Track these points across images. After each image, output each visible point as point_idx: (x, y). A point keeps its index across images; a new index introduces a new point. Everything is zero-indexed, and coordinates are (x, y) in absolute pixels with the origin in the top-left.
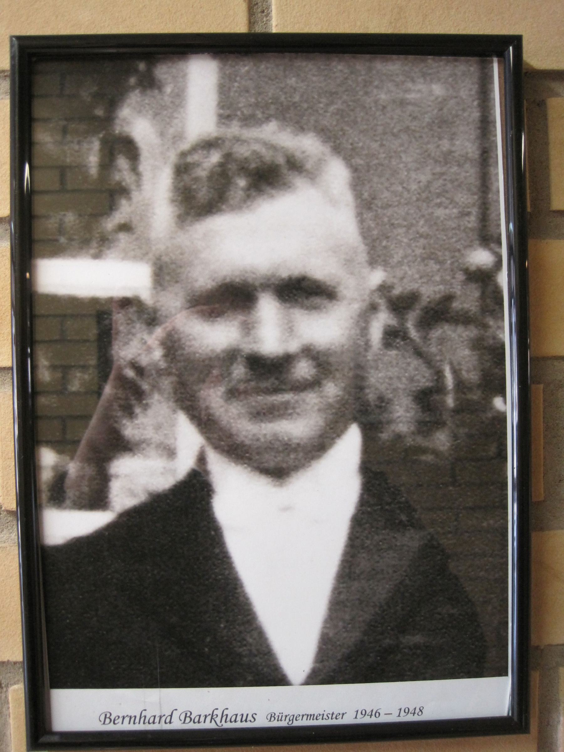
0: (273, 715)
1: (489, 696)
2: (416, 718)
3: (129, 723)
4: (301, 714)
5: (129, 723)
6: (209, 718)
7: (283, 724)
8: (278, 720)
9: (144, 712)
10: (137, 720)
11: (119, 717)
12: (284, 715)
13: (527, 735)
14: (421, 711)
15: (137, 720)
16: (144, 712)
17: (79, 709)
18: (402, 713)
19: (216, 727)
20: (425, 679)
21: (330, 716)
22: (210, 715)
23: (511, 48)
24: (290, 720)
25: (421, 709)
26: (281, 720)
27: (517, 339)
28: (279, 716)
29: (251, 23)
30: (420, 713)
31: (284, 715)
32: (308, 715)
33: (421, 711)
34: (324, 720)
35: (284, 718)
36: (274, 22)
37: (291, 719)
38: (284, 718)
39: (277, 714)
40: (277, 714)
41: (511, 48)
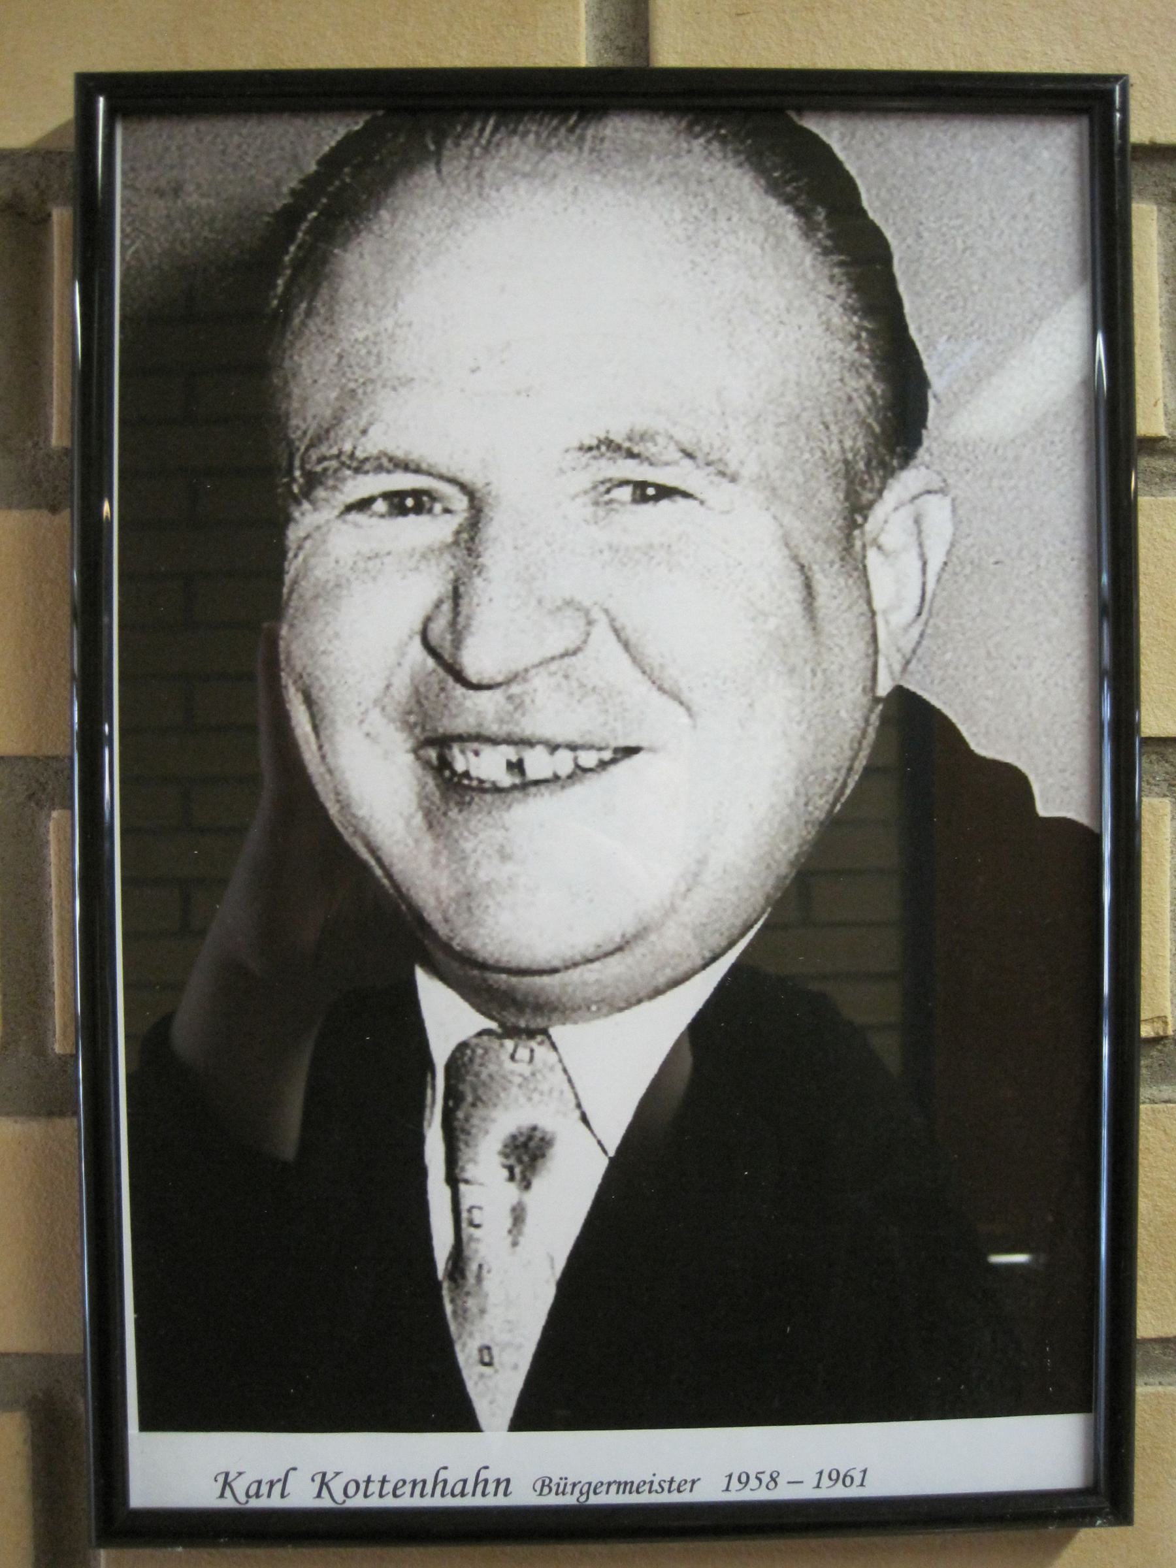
0: (547, 1482)
1: (1038, 1450)
2: (762, 1495)
3: (618, 1492)
4: (689, 1480)
5: (618, 1492)
6: (278, 1488)
7: (569, 1500)
8: (557, 1494)
9: (442, 1472)
10: (429, 1489)
11: (404, 1482)
12: (570, 1481)
13: (1130, 1528)
14: (773, 1479)
15: (429, 1489)
16: (442, 1472)
17: (176, 1469)
18: (825, 1481)
19: (236, 1505)
20: (955, 1417)
21: (666, 1486)
22: (279, 1480)
23: (101, 100)
24: (581, 1494)
25: (775, 1475)
26: (563, 1493)
27: (1112, 749)
28: (559, 1485)
29: (1147, 741)
30: (772, 1485)
31: (570, 1481)
32: (620, 1484)
33: (773, 1479)
34: (654, 1494)
35: (569, 1489)
36: (1147, 498)
37: (585, 1490)
38: (569, 1489)
39: (555, 1480)
40: (555, 1480)
41: (101, 100)
